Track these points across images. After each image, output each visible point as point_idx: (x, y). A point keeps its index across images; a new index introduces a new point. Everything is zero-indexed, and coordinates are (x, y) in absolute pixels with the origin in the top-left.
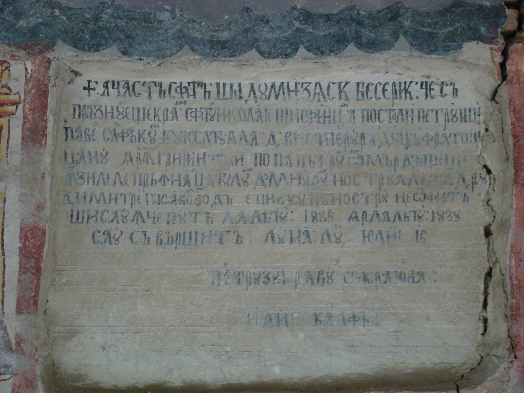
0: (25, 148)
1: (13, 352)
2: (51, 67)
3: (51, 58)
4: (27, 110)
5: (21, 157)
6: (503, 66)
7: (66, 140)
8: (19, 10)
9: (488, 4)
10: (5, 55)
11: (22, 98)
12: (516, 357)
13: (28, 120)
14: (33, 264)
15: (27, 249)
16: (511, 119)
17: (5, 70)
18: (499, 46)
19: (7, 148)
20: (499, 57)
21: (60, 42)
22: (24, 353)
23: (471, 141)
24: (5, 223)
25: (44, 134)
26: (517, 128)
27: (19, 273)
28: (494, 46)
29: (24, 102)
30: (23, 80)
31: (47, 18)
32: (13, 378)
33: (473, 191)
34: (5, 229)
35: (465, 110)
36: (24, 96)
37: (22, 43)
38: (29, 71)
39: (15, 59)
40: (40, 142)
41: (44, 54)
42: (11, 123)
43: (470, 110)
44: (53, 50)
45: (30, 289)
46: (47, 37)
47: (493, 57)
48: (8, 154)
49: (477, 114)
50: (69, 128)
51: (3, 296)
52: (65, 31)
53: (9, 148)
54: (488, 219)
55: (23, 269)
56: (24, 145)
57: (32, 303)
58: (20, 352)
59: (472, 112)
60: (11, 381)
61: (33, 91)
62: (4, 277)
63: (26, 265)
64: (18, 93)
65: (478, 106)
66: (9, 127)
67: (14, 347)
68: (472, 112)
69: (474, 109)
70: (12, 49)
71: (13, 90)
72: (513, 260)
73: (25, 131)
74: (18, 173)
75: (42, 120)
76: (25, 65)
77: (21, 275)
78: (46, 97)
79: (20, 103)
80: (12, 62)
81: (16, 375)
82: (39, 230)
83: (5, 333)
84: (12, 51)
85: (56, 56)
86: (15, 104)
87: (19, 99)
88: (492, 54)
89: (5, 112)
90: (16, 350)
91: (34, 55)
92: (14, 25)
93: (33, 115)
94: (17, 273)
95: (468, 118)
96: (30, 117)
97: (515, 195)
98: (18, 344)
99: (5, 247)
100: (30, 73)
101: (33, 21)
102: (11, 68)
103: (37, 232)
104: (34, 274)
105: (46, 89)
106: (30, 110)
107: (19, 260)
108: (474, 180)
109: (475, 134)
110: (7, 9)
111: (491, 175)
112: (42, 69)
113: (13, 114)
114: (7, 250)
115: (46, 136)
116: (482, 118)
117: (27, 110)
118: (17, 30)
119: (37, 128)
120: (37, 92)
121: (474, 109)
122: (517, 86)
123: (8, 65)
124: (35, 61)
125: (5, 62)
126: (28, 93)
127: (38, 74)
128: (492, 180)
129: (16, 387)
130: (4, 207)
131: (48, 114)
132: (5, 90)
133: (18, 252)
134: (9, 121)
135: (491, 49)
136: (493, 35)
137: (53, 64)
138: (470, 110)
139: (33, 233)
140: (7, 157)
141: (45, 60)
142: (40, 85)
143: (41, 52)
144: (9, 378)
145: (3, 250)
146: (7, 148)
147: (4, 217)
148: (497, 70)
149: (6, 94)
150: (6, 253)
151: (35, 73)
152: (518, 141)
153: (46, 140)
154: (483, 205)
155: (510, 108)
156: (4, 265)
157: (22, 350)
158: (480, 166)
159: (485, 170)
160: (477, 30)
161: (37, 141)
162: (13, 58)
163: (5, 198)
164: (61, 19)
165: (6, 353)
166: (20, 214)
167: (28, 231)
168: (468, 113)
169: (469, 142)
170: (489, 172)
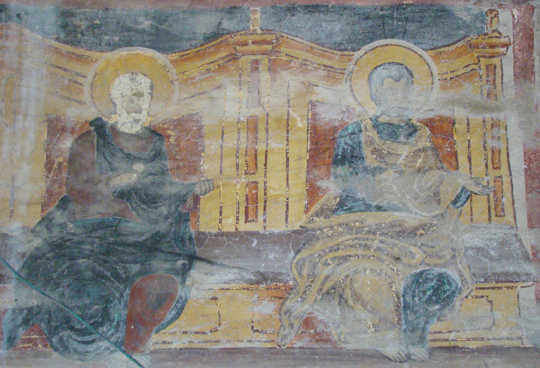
0: (517, 83)
1: (531, 261)
2: (534, 14)
3: (535, 6)
4: (517, 51)
5: (515, 91)
11: (512, 41)
13: (518, 59)
15: (532, 171)
17: (494, 17)
19: (502, 83)
24: (509, 147)
25: (532, 71)
27: (526, 192)
29: (514, 44)
30: (511, 25)
32: (535, 285)
34: (510, 152)
36: (514, 39)
38: (516, 17)
40: (530, 78)
48: (503, 89)
51: (515, 212)
53: (504, 84)
56: (516, 81)
60: (533, 288)
61: (521, 34)
62: (513, 196)
63: (531, 184)
64: (508, 36)
66: (501, 65)
67: (531, 257)
71: (502, 33)
73: (517, 68)
75: (530, 59)
76: (512, 12)
77: (528, 194)
78: (532, 40)
79: (510, 45)
80: (500, 10)
83: (521, 245)
87: (509, 41)
90: (533, 260)
93: (523, 55)
94: (524, 192)
96: (520, 57)
98: (534, 254)
99: (512, 169)
100: (517, 19)
102: (499, 16)
105: (531, 32)
106: (519, 50)
107: (524, 181)
112: (527, 15)
113: (505, 55)
114: (514, 172)
115: (534, 73)
117: (517, 51)
119: (526, 66)
120: (524, 35)
124: (520, 9)
125: (494, 10)
126: (517, 36)
127: (524, 20)
130: (506, 134)
131: (534, 54)
132: (496, 34)
133: (523, 173)
134: (501, 60)
137: (536, 11)
139: (535, 156)
140: (503, 91)
141: (529, 8)
142: (526, 29)
144: (532, 285)
145: (510, 171)
146: (502, 83)
147: (507, 143)
149: (497, 37)
151: (521, 19)
153: (535, 77)
161: (528, 78)
162: (500, 6)
163: (506, 126)
165: (525, 263)
166: (522, 139)
167: (531, 154)
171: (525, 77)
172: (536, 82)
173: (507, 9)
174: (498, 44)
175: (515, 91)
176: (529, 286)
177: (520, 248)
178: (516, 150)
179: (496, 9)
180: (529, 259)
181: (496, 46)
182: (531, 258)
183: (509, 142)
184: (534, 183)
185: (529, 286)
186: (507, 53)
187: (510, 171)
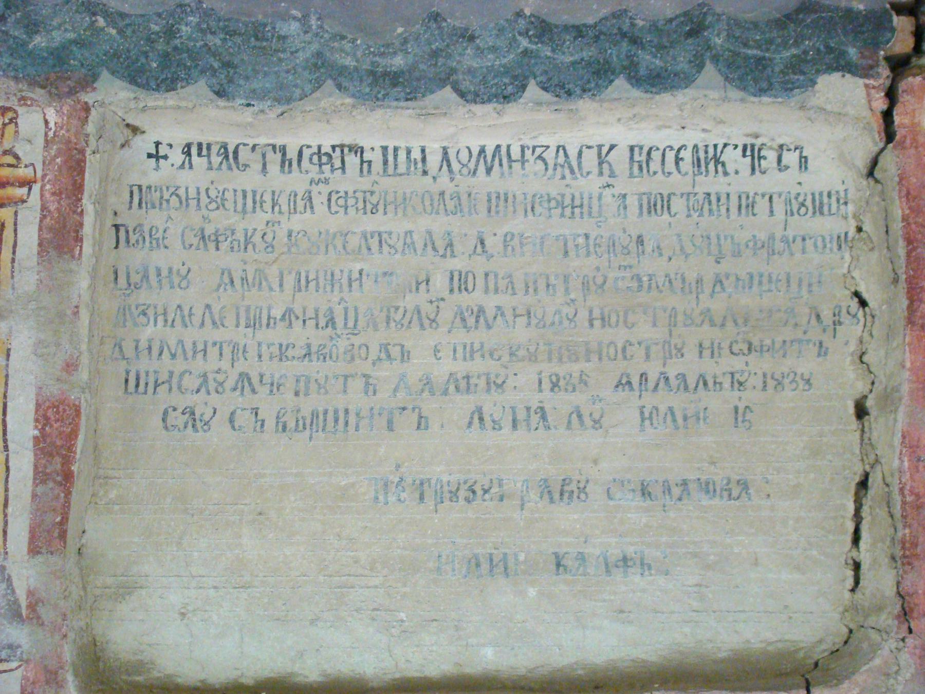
0: (44, 261)
1: (23, 621)
2: (90, 118)
3: (91, 102)
4: (47, 195)
5: (37, 277)
6: (887, 116)
7: (116, 247)
9: (861, 7)
10: (8, 98)
11: (39, 174)
12: (910, 631)
13: (50, 211)
14: (59, 467)
15: (48, 440)
16: (903, 209)
17: (9, 123)
18: (881, 81)
19: (13, 260)
20: (881, 101)
21: (105, 75)
22: (43, 624)
23: (831, 250)
24: (8, 394)
25: (77, 236)
26: (913, 226)
27: (34, 483)
28: (871, 82)
29: (43, 181)
30: (40, 141)
32: (22, 667)
33: (834, 337)
34: (9, 404)
35: (821, 194)
36: (43, 170)
38: (52, 125)
39: (26, 105)
40: (71, 251)
41: (78, 95)
42: (19, 218)
43: (829, 195)
44: (94, 89)
45: (54, 510)
46: (82, 65)
47: (869, 102)
48: (13, 272)
49: (842, 201)
50: (123, 225)
51: (6, 523)
52: (115, 54)
53: (16, 261)
54: (861, 387)
55: (40, 476)
56: (42, 257)
58: (35, 621)
59: (834, 198)
60: (19, 673)
61: (58, 160)
62: (7, 490)
63: (45, 467)
64: (33, 164)
65: (844, 187)
66: (15, 224)
67: (24, 612)
68: (834, 198)
69: (837, 192)
70: (20, 86)
71: (22, 158)
72: (906, 459)
73: (45, 231)
74: (33, 305)
75: (74, 212)
76: (45, 115)
77: (37, 486)
78: (82, 172)
79: (35, 182)
80: (21, 110)
81: (27, 661)
82: (69, 406)
84: (21, 91)
86: (27, 183)
88: (868, 95)
89: (9, 198)
90: (28, 617)
91: (60, 97)
92: (24, 44)
93: (59, 203)
95: (826, 209)
96: (53, 207)
97: (909, 344)
98: (32, 607)
99: (9, 437)
100: (53, 129)
101: (58, 37)
102: (19, 121)
106: (53, 194)
107: (33, 460)
108: (837, 318)
109: (839, 237)
110: (13, 16)
111: (867, 309)
112: (75, 122)
113: (24, 201)
115: (81, 240)
116: (851, 208)
117: (47, 195)
119: (64, 227)
120: (65, 162)
121: (837, 192)
122: (913, 151)
124: (61, 108)
125: (9, 109)
126: (49, 164)
127: (68, 131)
128: (869, 318)
129: (29, 683)
130: (7, 365)
131: (84, 201)
132: (9, 159)
133: (31, 444)
134: (16, 213)
135: (866, 86)
136: (870, 62)
137: (93, 112)
138: (829, 195)
139: (58, 412)
140: (13, 277)
141: (79, 106)
142: (70, 149)
143: (72, 92)
144: (16, 668)
145: (5, 441)
146: (13, 260)
147: (6, 384)
148: (877, 123)
149: (10, 166)
150: (11, 446)
151: (62, 128)
152: (915, 249)
153: (81, 247)
154: (853, 362)
155: (900, 191)
157: (39, 618)
158: (847, 293)
159: (856, 300)
160: (843, 54)
161: (66, 250)
162: (22, 102)
163: (9, 350)
164: (107, 34)
165: (10, 623)
166: (36, 378)
167: (49, 408)
168: (825, 200)
169: (827, 250)
170: (863, 303)
171: (60, 249)
172: (84, 258)
173: (34, 108)
174: (11, 181)
175: (37, 277)
176: (11, 670)
177: (7, 594)
178: (21, 400)
179: (13, 107)
180: (20, 615)
181: (8, 183)
182: (24, 614)
183: (10, 382)
184: (51, 464)
185: (11, 670)
186: (28, 198)
187: (5, 441)
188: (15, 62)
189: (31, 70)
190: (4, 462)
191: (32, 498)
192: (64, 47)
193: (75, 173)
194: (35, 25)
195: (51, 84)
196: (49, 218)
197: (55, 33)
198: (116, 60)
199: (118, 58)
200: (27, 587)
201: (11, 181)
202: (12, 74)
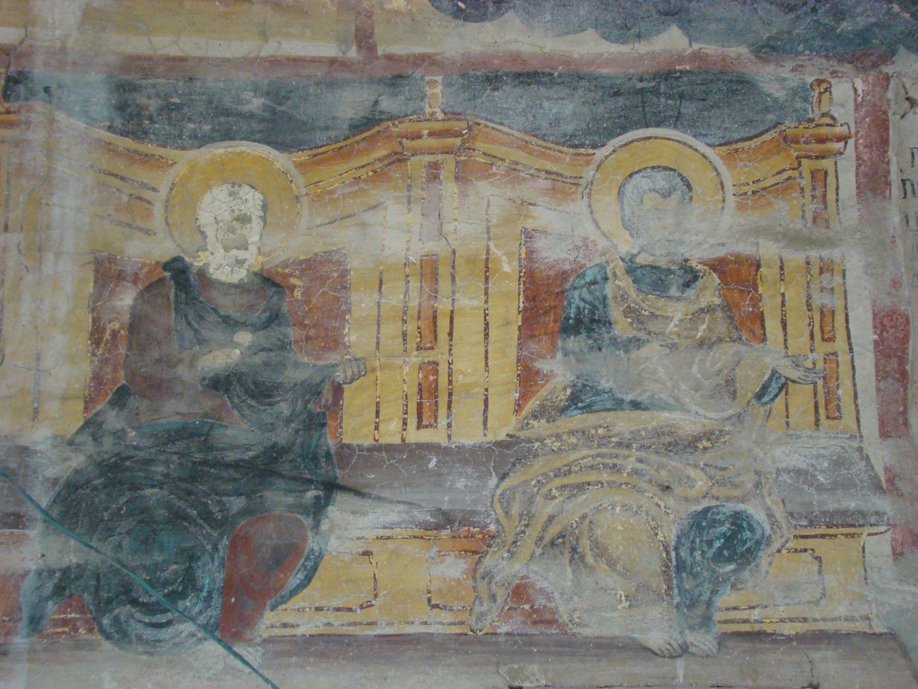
1: (885, 492)
2: (890, 86)
3: (890, 74)
4: (861, 148)
5: (859, 213)
7: (905, 197)
8: (839, 7)
10: (822, 72)
11: (853, 131)
13: (864, 161)
14: (896, 366)
15: (886, 344)
19: (837, 201)
21: (902, 50)
22: (902, 495)
24: (848, 306)
27: (876, 379)
30: (851, 105)
31: (881, 17)
32: (891, 531)
36: (856, 127)
37: (847, 54)
38: (860, 92)
39: (837, 76)
40: (883, 193)
41: (880, 67)
42: (839, 166)
44: (893, 63)
45: (896, 401)
46: (882, 44)
50: (909, 180)
51: (858, 412)
52: (909, 33)
55: (881, 374)
57: (901, 422)
58: (895, 492)
60: (888, 535)
61: (868, 120)
62: (855, 385)
63: (885, 366)
64: (847, 124)
66: (836, 171)
70: (831, 62)
74: (858, 236)
75: (883, 162)
77: (879, 381)
78: (887, 129)
79: (850, 137)
80: (833, 81)
81: (894, 526)
82: (900, 315)
84: (832, 66)
85: (898, 70)
86: (844, 139)
87: (848, 132)
89: (828, 151)
91: (864, 69)
92: (833, 29)
93: (871, 154)
94: (874, 379)
96: (866, 157)
98: (890, 481)
99: (852, 341)
100: (861, 95)
101: (861, 22)
102: (833, 90)
103: (897, 319)
104: (898, 380)
106: (866, 147)
107: (873, 360)
110: (823, 8)
112: (878, 89)
113: (841, 154)
114: (857, 345)
115: (890, 184)
117: (861, 148)
118: (839, 36)
119: (876, 173)
120: (873, 121)
123: (829, 86)
125: (824, 81)
126: (861, 122)
127: (873, 96)
129: (898, 544)
130: (844, 283)
132: (827, 120)
133: (871, 347)
134: (836, 163)
137: (892, 81)
139: (892, 320)
140: (838, 214)
141: (881, 77)
142: (875, 111)
143: (875, 65)
144: (886, 532)
146: (837, 201)
147: (846, 298)
150: (855, 348)
151: (868, 95)
153: (890, 190)
156: (853, 368)
157: (897, 490)
161: (879, 192)
163: (844, 271)
164: (902, 18)
166: (870, 293)
167: (884, 316)
171: (874, 191)
175: (859, 213)
176: (881, 533)
180: (881, 488)
181: (827, 139)
182: (885, 488)
185: (881, 533)
186: (845, 150)
188: (826, 44)
189: (840, 49)
190: (850, 362)
191: (877, 392)
192: (866, 29)
193: (882, 130)
194: (841, 13)
195: (857, 60)
196: (863, 167)
197: (858, 19)
198: (910, 38)
199: (913, 36)
200: (883, 465)
201: (830, 137)
202: (824, 53)
